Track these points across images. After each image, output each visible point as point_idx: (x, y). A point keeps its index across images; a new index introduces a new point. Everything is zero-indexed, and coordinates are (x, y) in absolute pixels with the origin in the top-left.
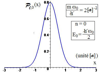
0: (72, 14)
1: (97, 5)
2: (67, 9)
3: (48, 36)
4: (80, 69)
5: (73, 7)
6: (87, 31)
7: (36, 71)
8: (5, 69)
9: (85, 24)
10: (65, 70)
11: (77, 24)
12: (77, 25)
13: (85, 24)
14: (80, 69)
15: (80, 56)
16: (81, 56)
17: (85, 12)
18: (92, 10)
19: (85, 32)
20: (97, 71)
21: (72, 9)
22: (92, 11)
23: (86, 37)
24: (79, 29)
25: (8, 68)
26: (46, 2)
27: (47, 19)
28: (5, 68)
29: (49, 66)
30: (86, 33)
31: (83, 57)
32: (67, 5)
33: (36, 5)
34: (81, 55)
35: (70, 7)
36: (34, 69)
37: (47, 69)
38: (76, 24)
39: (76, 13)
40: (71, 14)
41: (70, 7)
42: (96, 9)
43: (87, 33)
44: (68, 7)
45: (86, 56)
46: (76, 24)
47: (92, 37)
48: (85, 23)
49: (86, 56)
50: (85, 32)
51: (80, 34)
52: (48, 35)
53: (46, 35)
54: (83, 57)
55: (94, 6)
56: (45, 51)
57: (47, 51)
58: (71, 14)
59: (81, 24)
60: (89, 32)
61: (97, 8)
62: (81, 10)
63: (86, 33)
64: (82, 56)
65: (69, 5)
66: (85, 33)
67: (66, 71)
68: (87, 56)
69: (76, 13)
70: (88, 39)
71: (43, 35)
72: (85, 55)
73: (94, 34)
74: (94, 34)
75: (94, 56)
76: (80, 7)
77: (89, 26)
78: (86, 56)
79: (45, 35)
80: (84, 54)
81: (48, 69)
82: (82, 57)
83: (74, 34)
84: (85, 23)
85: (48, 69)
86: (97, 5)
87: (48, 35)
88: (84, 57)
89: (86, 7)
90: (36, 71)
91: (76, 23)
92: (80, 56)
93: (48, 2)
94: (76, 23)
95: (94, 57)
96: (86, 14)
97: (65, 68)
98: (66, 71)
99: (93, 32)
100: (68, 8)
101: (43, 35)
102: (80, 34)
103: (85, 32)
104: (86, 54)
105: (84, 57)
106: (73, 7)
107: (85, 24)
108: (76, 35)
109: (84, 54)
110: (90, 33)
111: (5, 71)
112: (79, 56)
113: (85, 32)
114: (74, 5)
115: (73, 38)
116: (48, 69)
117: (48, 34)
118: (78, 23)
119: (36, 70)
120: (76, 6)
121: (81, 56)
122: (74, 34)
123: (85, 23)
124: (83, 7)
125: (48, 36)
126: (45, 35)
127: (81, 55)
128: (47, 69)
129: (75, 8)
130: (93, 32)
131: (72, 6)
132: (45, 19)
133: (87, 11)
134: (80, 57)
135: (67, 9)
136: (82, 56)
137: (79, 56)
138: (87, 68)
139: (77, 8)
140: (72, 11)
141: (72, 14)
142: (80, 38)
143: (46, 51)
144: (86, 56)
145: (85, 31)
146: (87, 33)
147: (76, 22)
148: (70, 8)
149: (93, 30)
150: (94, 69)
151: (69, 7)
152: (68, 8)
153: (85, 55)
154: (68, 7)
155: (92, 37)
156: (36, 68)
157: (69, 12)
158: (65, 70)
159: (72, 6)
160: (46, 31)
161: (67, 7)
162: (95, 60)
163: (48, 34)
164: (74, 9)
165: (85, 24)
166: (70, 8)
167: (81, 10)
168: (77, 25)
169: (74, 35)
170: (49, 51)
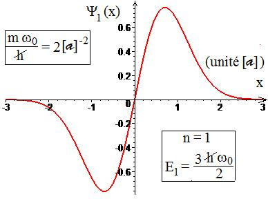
0: (20, 58)
1: (87, 34)
2: (8, 44)
3: (129, 54)
4: (219, 105)
5: (25, 39)
6: (215, 157)
7: (94, 109)
8: (9, 105)
10: (177, 105)
11: (187, 138)
14: (219, 105)
15: (218, 64)
16: (218, 63)
17: (55, 51)
18: (74, 46)
19: (210, 160)
20: (264, 109)
21: (21, 43)
22: (74, 50)
23: (212, 173)
26: (122, 26)
27: (127, 29)
28: (8, 102)
30: (212, 162)
31: (225, 64)
32: (8, 33)
33: (108, 12)
34: (219, 60)
35: (15, 38)
37: (127, 105)
39: (31, 55)
40: (20, 56)
41: (15, 38)
42: (85, 43)
43: (216, 162)
44: (11, 38)
45: (232, 64)
46: (186, 139)
47: (228, 173)
49: (232, 64)
50: (210, 160)
51: (185, 166)
53: (122, 51)
54: (225, 64)
55: (80, 37)
56: (120, 52)
57: (127, 74)
58: (20, 56)
59: (197, 138)
60: (220, 159)
61: (88, 41)
62: (46, 47)
63: (212, 162)
64: (221, 62)
65: (14, 33)
66: (210, 164)
67: (178, 109)
68: (236, 64)
69: (31, 55)
70: (218, 178)
72: (230, 60)
73: (233, 164)
74: (233, 164)
75: (254, 61)
76: (43, 38)
77: (220, 145)
78: (232, 62)
80: (227, 58)
85: (130, 103)
86: (87, 34)
87: (128, 52)
88: (227, 66)
89: (59, 37)
90: (94, 109)
91: (185, 136)
92: (218, 64)
94: (185, 136)
95: (254, 66)
96: (60, 58)
97: (176, 102)
98: (178, 109)
99: (230, 161)
100: (11, 40)
102: (185, 166)
103: (210, 160)
104: (234, 59)
105: (227, 66)
106: (25, 37)
109: (228, 59)
110: (222, 163)
111: (9, 109)
112: (214, 64)
113: (210, 160)
114: (27, 33)
115: (167, 176)
117: (129, 49)
118: (191, 135)
119: (93, 105)
120: (33, 35)
121: (218, 63)
122: (169, 164)
125: (129, 54)
127: (219, 60)
128: (127, 103)
129: (28, 40)
130: (230, 161)
131: (20, 35)
132: (120, 172)
133: (61, 48)
134: (216, 65)
135: (8, 44)
136: (221, 62)
137: (214, 64)
139: (34, 41)
140: (21, 50)
141: (20, 58)
142: (184, 174)
143: (122, 123)
144: (232, 62)
146: (216, 162)
147: (186, 133)
148: (15, 40)
149: (230, 154)
150: (258, 105)
151: (13, 39)
152: (11, 40)
153: (230, 60)
154: (11, 38)
155: (228, 173)
156: (93, 102)
157: (12, 52)
158: (177, 105)
159: (20, 35)
161: (7, 38)
162: (259, 74)
163: (129, 49)
164: (26, 44)
166: (15, 40)
167: (46, 47)
169: (170, 169)
170: (132, 73)
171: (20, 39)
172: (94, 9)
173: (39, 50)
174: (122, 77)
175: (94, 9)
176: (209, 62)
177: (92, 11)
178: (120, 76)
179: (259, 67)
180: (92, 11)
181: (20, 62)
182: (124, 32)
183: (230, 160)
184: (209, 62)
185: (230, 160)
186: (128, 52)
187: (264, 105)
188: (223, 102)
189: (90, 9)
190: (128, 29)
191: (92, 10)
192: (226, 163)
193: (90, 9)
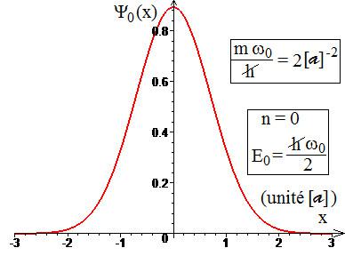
1: (336, 44)
2: (234, 57)
3: (166, 136)
4: (277, 240)
5: (256, 51)
7: (123, 246)
8: (18, 240)
9: (295, 121)
10: (226, 241)
11: (266, 119)
12: (268, 124)
13: (295, 120)
14: (277, 240)
15: (277, 200)
17: (295, 66)
18: (319, 59)
19: (296, 148)
20: (333, 245)
21: (251, 55)
22: (319, 65)
23: (298, 164)
24: (274, 138)
25: (25, 234)
26: (157, 80)
27: (163, 83)
28: (17, 236)
29: (169, 229)
31: (286, 201)
32: (235, 43)
33: (142, 13)
34: (279, 196)
35: (244, 49)
36: (118, 239)
37: (163, 240)
38: (266, 121)
39: (264, 71)
40: (249, 72)
41: (244, 49)
42: (334, 56)
43: (304, 150)
44: (239, 49)
45: (295, 200)
46: (266, 121)
47: (319, 164)
48: (295, 116)
49: (295, 200)
50: (296, 148)
51: (278, 155)
52: (165, 133)
53: (157, 131)
54: (286, 201)
55: (326, 47)
56: (155, 132)
57: (163, 180)
58: (249, 72)
59: (280, 118)
60: (309, 146)
61: (338, 53)
62: (283, 60)
64: (281, 198)
65: (242, 43)
67: (226, 246)
68: (300, 200)
69: (264, 71)
70: (306, 170)
71: (147, 80)
72: (293, 195)
73: (326, 153)
74: (326, 153)
75: (324, 197)
76: (279, 49)
77: (311, 128)
79: (155, 82)
80: (288, 193)
81: (165, 238)
82: (284, 203)
83: (257, 153)
84: (295, 116)
85: (167, 237)
86: (336, 44)
88: (288, 203)
89: (301, 48)
90: (123, 246)
91: (263, 117)
92: (277, 200)
93: (167, 29)
94: (263, 117)
95: (324, 203)
96: (301, 75)
97: (224, 237)
98: (226, 246)
99: (322, 149)
100: (239, 51)
101: (147, 80)
102: (278, 155)
103: (296, 148)
104: (297, 194)
105: (288, 203)
106: (256, 49)
107: (295, 121)
108: (262, 157)
109: (290, 194)
110: (312, 152)
111: (18, 245)
112: (272, 200)
113: (296, 148)
114: (258, 43)
116: (165, 238)
117: (166, 129)
118: (272, 114)
119: (123, 241)
120: (266, 44)
122: (257, 153)
123: (295, 117)
124: (288, 50)
125: (166, 136)
126: (155, 82)
127: (279, 196)
128: (163, 237)
130: (322, 149)
131: (250, 45)
133: (302, 62)
134: (274, 202)
135: (234, 57)
136: (281, 198)
137: (272, 200)
138: (321, 234)
139: (267, 53)
140: (251, 64)
142: (275, 166)
145: (295, 144)
146: (304, 150)
147: (265, 113)
148: (244, 52)
149: (322, 139)
150: (326, 240)
151: (241, 50)
152: (239, 51)
154: (239, 49)
155: (319, 164)
156: (123, 236)
157: (239, 68)
158: (226, 241)
159: (250, 45)
160: (159, 68)
163: (166, 129)
164: (258, 57)
165: (295, 120)
166: (244, 52)
167: (283, 60)
168: (268, 124)
169: (258, 158)
170: (170, 180)
171: (250, 50)
172: (123, 9)
173: (274, 64)
174: (157, 185)
175: (123, 9)
176: (266, 199)
177: (121, 12)
178: (155, 183)
179: (330, 203)
180: (121, 12)
181: (250, 80)
182: (160, 87)
183: (322, 147)
184: (266, 199)
185: (322, 147)
186: (165, 133)
187: (333, 240)
188: (281, 236)
189: (119, 9)
190: (165, 83)
191: (121, 10)
192: (317, 151)
193: (119, 9)
